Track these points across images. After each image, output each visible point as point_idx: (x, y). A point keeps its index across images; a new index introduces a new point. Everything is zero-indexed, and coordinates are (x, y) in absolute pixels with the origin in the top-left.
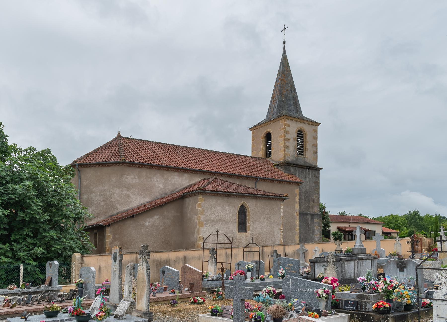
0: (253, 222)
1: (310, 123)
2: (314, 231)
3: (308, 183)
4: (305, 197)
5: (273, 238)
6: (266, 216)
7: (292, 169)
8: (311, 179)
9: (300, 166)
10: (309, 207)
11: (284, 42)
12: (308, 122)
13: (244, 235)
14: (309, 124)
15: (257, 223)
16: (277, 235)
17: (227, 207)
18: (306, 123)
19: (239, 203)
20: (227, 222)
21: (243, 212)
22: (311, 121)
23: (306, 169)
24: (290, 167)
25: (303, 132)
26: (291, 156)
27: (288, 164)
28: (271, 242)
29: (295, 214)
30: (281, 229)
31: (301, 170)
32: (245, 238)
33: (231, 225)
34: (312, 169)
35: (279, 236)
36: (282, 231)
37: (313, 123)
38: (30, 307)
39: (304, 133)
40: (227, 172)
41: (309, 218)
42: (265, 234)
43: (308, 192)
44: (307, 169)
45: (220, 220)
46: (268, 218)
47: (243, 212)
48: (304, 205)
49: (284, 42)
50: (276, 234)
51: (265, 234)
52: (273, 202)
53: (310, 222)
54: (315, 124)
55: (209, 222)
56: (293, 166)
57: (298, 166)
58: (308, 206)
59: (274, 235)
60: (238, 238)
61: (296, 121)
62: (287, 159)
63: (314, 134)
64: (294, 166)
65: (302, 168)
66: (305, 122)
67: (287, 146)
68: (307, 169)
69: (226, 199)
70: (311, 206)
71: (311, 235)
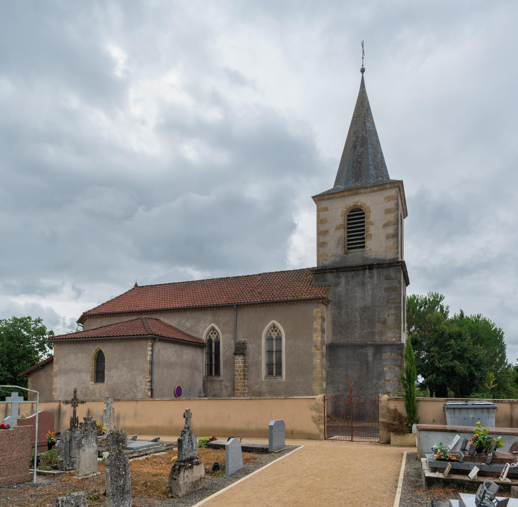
0: (109, 371)
1: (376, 189)
2: (381, 375)
3: (370, 293)
4: (361, 317)
5: (134, 390)
6: (126, 362)
7: (331, 277)
8: (377, 284)
9: (348, 269)
10: (373, 334)
11: (363, 71)
12: (369, 190)
13: (99, 385)
14: (374, 191)
15: (114, 371)
16: (141, 385)
17: (80, 355)
18: (365, 193)
19: (92, 349)
20: (80, 371)
21: (100, 358)
22: (394, 181)
23: (365, 269)
24: (327, 274)
25: (362, 209)
26: (331, 256)
27: (332, 269)
28: (132, 394)
29: (313, 348)
30: (147, 378)
31: (350, 275)
32: (100, 389)
33: (84, 374)
34: (378, 268)
35: (143, 386)
36: (148, 380)
37: (382, 187)
38: (141, 445)
39: (364, 210)
40: (104, 312)
41: (370, 352)
42: (124, 385)
43: (369, 309)
44: (368, 270)
45: (72, 370)
46: (128, 364)
47: (100, 358)
48: (360, 331)
49: (363, 71)
50: (138, 384)
51: (124, 385)
52: (136, 344)
53: (370, 359)
54: (388, 186)
55: (63, 372)
56: (331, 272)
57: (340, 270)
58: (369, 333)
59: (136, 386)
60: (91, 389)
61: (341, 197)
62: (323, 263)
63: (323, 215)
64: (334, 272)
65: (352, 271)
66: (363, 191)
67: (323, 243)
68: (368, 270)
69: (79, 346)
70: (377, 331)
71: (375, 381)
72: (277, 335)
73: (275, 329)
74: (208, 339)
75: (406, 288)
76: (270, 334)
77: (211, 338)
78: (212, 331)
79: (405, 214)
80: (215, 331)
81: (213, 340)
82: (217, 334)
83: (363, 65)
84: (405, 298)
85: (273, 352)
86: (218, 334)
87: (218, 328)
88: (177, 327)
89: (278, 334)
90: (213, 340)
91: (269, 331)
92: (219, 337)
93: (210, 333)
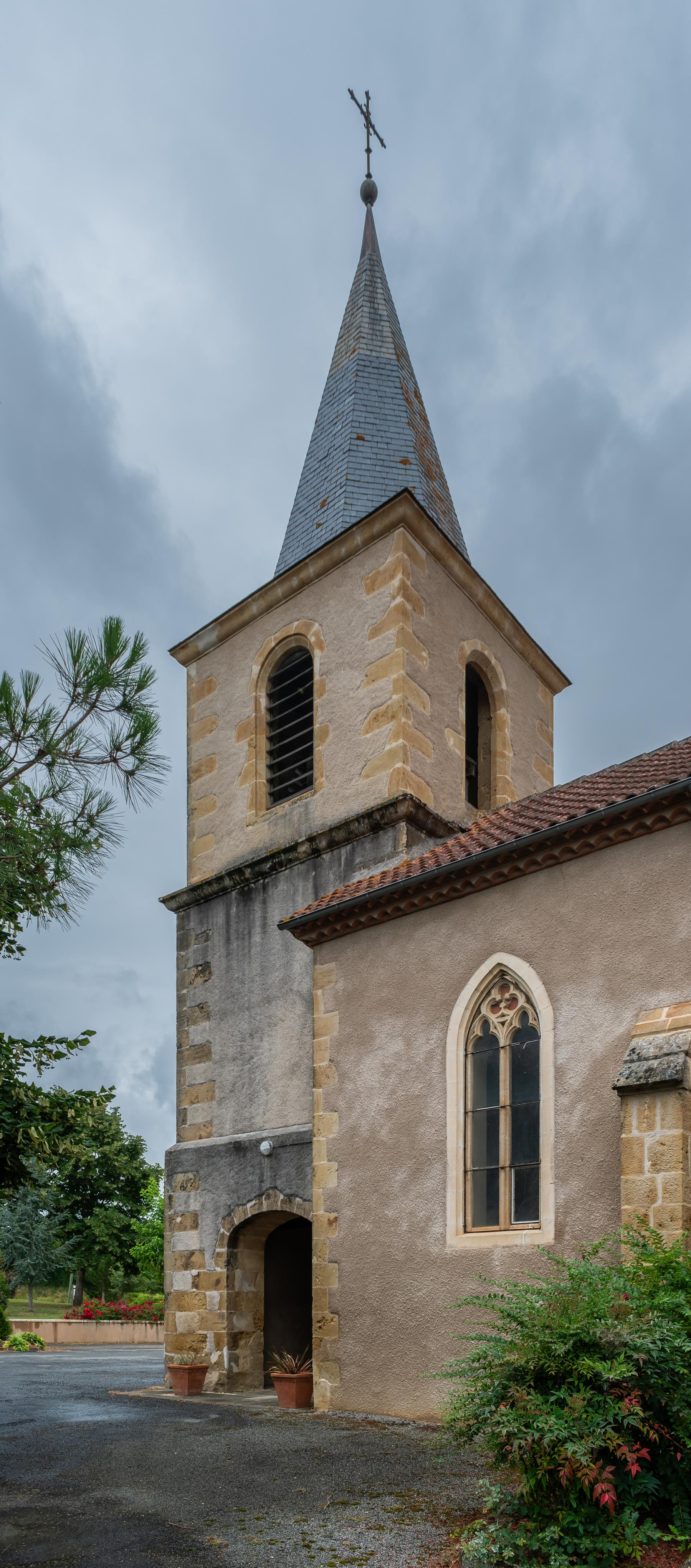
11: (369, 194)
49: (369, 194)
72: (516, 1024)
73: (507, 996)
74: (479, 1039)
75: (552, 699)
76: (486, 1023)
77: (492, 1029)
78: (496, 995)
79: (189, 651)
80: (512, 990)
81: (502, 1043)
82: (522, 1001)
83: (369, 176)
84: (107, 1349)
85: (472, 1054)
86: (528, 1000)
87: (477, 973)
88: (462, 728)
89: (524, 1015)
90: (503, 1037)
91: (479, 1011)
92: (537, 1018)
93: (485, 1010)
